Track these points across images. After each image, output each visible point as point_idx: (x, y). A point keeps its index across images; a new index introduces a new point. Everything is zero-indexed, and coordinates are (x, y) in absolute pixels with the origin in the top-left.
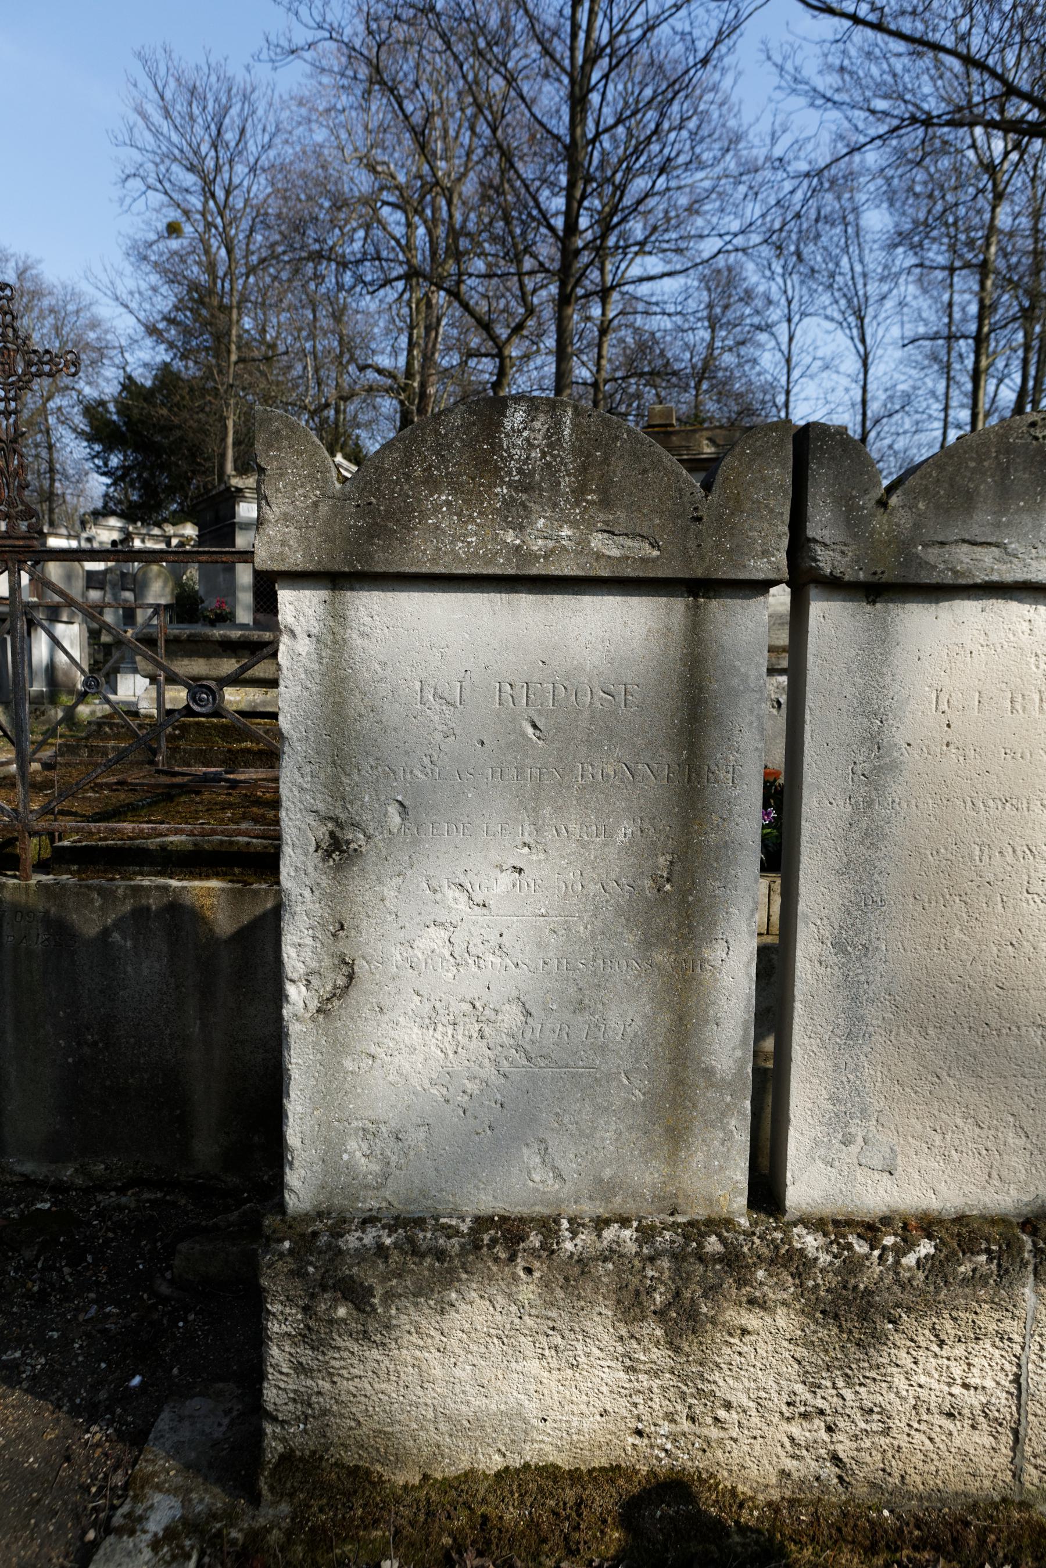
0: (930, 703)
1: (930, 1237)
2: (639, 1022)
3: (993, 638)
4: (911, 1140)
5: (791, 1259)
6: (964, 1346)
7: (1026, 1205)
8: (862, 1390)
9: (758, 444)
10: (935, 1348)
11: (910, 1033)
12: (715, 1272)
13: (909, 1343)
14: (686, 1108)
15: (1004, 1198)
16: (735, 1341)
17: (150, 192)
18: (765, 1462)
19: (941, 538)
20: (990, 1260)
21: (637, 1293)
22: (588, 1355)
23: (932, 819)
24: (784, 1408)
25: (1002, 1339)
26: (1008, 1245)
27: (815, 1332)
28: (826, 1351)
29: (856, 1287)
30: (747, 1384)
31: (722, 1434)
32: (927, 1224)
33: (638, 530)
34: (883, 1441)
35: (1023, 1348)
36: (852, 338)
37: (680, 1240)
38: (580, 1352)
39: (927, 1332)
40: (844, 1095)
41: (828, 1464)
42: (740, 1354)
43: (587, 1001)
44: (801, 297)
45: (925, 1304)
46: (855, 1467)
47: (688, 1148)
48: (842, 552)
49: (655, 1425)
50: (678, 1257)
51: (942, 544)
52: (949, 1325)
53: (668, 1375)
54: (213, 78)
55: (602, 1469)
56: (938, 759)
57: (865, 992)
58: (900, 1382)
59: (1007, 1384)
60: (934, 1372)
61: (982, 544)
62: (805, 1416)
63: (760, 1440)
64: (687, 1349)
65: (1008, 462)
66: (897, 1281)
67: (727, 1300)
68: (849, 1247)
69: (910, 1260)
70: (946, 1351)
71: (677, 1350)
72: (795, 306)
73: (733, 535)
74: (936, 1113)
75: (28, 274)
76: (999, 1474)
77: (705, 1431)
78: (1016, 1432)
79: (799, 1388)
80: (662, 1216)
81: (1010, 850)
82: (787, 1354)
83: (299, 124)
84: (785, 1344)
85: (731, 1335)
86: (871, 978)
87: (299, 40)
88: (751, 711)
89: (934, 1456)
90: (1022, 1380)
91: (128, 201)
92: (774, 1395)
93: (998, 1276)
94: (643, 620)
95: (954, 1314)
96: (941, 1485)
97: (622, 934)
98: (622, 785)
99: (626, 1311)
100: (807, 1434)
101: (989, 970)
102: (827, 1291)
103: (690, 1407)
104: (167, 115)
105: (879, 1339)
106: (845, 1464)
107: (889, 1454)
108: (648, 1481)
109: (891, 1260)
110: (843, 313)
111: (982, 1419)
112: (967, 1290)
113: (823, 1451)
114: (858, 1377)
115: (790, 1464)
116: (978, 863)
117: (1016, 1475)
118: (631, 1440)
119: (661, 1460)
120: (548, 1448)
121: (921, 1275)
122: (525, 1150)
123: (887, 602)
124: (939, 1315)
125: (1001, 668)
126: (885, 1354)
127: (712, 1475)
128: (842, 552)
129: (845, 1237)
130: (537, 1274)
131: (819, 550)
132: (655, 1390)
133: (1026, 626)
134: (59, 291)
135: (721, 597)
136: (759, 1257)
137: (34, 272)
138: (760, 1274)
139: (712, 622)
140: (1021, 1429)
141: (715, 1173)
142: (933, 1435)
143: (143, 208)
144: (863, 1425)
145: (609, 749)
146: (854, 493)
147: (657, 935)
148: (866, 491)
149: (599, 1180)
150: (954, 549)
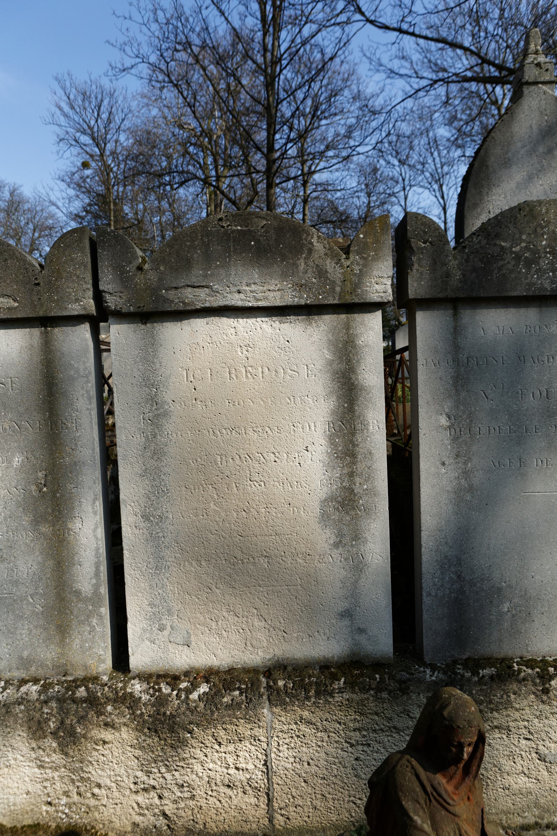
0: (183, 377)
1: (207, 682)
2: (35, 567)
3: (215, 338)
4: (198, 626)
5: (125, 699)
6: (233, 745)
7: (269, 660)
8: (176, 774)
9: (67, 241)
10: (216, 747)
11: (191, 564)
12: (83, 708)
13: (201, 745)
15: (256, 657)
16: (100, 748)
17: (72, 148)
18: (123, 818)
19: (175, 285)
20: (241, 694)
21: (39, 722)
22: (15, 759)
23: (191, 442)
24: (132, 786)
25: (255, 740)
26: (252, 685)
27: (145, 741)
28: (153, 751)
29: (164, 714)
30: (109, 773)
31: (97, 803)
32: (208, 675)
33: (5, 292)
34: (191, 803)
35: (268, 745)
36: (436, 197)
37: (63, 690)
38: (10, 758)
39: (210, 738)
40: (157, 602)
41: (161, 818)
42: (103, 755)
43: (5, 556)
44: (410, 176)
45: (207, 722)
46: (176, 819)
47: (70, 637)
48: (120, 297)
49: (59, 799)
50: (61, 700)
51: (176, 288)
52: (222, 733)
53: (63, 769)
54: (94, 87)
55: (29, 826)
56: (191, 408)
57: (163, 543)
58: (198, 768)
59: (261, 766)
60: (217, 761)
61: (198, 287)
63: (120, 805)
64: (72, 754)
65: (209, 241)
66: (188, 709)
68: (160, 690)
69: (194, 696)
71: (66, 754)
72: (407, 182)
73: (58, 292)
74: (211, 610)
75: (15, 193)
76: (261, 820)
77: (87, 801)
78: (268, 795)
79: (139, 774)
80: (59, 677)
81: (238, 457)
82: (130, 754)
83: (143, 107)
84: (129, 748)
85: (96, 744)
86: (166, 534)
87: (128, 64)
88: (83, 388)
89: (222, 811)
90: (268, 764)
91: (61, 152)
92: (125, 779)
93: (247, 703)
94: (17, 342)
95: (224, 726)
96: (227, 828)
97: (21, 517)
98: (14, 434)
99: (34, 733)
100: (147, 801)
101: (233, 526)
102: (149, 716)
103: (78, 787)
104: (72, 108)
105: (183, 743)
106: (170, 818)
107: (196, 811)
108: (56, 832)
109: (183, 696)
110: (430, 184)
111: (248, 788)
112: (229, 712)
113: (157, 811)
115: (138, 819)
116: (220, 465)
117: (271, 820)
118: (44, 808)
119: (63, 819)
121: (202, 705)
123: (152, 322)
125: (221, 355)
126: (187, 751)
127: (93, 827)
128: (120, 297)
129: (158, 684)
131: (108, 297)
132: (56, 778)
133: (233, 331)
134: (32, 200)
135: (60, 326)
136: (107, 698)
137: (18, 191)
138: (109, 708)
139: (56, 341)
140: (270, 793)
141: (87, 651)
142: (221, 799)
143: (70, 155)
144: (179, 794)
145: (5, 414)
146: (124, 264)
147: (41, 516)
148: (130, 262)
149: (21, 658)
150: (183, 291)
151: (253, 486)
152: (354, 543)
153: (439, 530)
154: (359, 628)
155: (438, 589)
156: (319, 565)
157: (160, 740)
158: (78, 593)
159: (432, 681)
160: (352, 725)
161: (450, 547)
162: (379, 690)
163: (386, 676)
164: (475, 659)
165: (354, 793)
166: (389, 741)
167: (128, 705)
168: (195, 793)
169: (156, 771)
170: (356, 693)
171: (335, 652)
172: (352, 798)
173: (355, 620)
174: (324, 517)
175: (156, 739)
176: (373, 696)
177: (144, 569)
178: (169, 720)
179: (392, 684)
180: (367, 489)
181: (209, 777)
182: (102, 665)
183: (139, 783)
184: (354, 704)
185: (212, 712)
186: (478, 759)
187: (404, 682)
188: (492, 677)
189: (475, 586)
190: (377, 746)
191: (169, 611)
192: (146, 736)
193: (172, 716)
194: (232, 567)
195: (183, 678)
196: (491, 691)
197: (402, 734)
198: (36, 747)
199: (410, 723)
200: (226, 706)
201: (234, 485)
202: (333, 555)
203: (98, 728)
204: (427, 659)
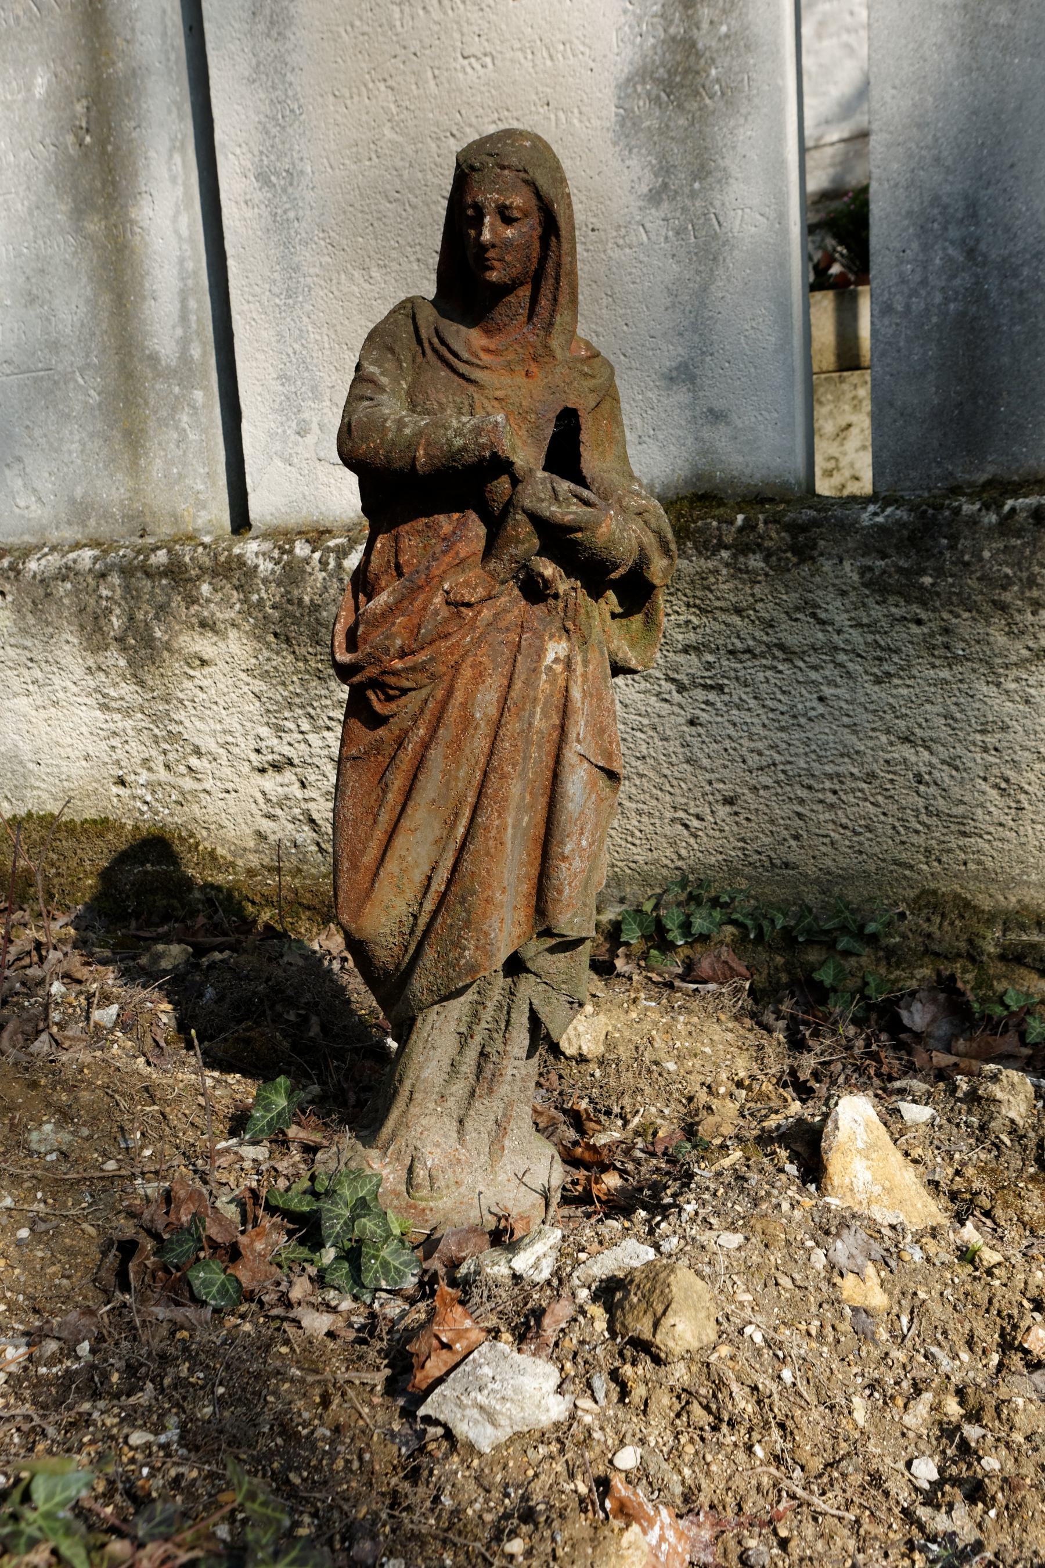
11: (352, 279)
14: (138, 406)
22: (65, 689)
24: (253, 757)
27: (269, 659)
28: (284, 684)
29: (300, 600)
31: (197, 786)
40: (292, 372)
47: (146, 454)
50: (127, 572)
53: (140, 716)
55: (95, 821)
68: (290, 552)
71: (141, 683)
79: (264, 731)
82: (246, 689)
92: (241, 740)
101: (430, 176)
102: (273, 607)
109: (332, 564)
115: (266, 825)
120: (45, 796)
122: (7, 472)
127: (192, 835)
130: (9, 598)
149: (72, 501)
151: (469, 70)
152: (697, 185)
153: (919, 126)
154: (711, 410)
155: (914, 293)
156: (615, 254)
158: (153, 359)
159: (875, 525)
160: (680, 637)
161: (948, 170)
162: (742, 549)
165: (684, 800)
166: (768, 681)
169: (293, 726)
170: (689, 558)
171: (656, 472)
172: (681, 814)
173: (702, 389)
174: (628, 125)
175: (290, 658)
176: (727, 565)
177: (264, 299)
179: (774, 535)
180: (727, 36)
182: (202, 513)
184: (683, 585)
186: (551, 281)
187: (804, 528)
189: (1015, 274)
190: (739, 692)
191: (314, 389)
193: (315, 608)
196: (1033, 553)
197: (801, 664)
198: (94, 666)
199: (820, 635)
201: (430, 74)
202: (648, 225)
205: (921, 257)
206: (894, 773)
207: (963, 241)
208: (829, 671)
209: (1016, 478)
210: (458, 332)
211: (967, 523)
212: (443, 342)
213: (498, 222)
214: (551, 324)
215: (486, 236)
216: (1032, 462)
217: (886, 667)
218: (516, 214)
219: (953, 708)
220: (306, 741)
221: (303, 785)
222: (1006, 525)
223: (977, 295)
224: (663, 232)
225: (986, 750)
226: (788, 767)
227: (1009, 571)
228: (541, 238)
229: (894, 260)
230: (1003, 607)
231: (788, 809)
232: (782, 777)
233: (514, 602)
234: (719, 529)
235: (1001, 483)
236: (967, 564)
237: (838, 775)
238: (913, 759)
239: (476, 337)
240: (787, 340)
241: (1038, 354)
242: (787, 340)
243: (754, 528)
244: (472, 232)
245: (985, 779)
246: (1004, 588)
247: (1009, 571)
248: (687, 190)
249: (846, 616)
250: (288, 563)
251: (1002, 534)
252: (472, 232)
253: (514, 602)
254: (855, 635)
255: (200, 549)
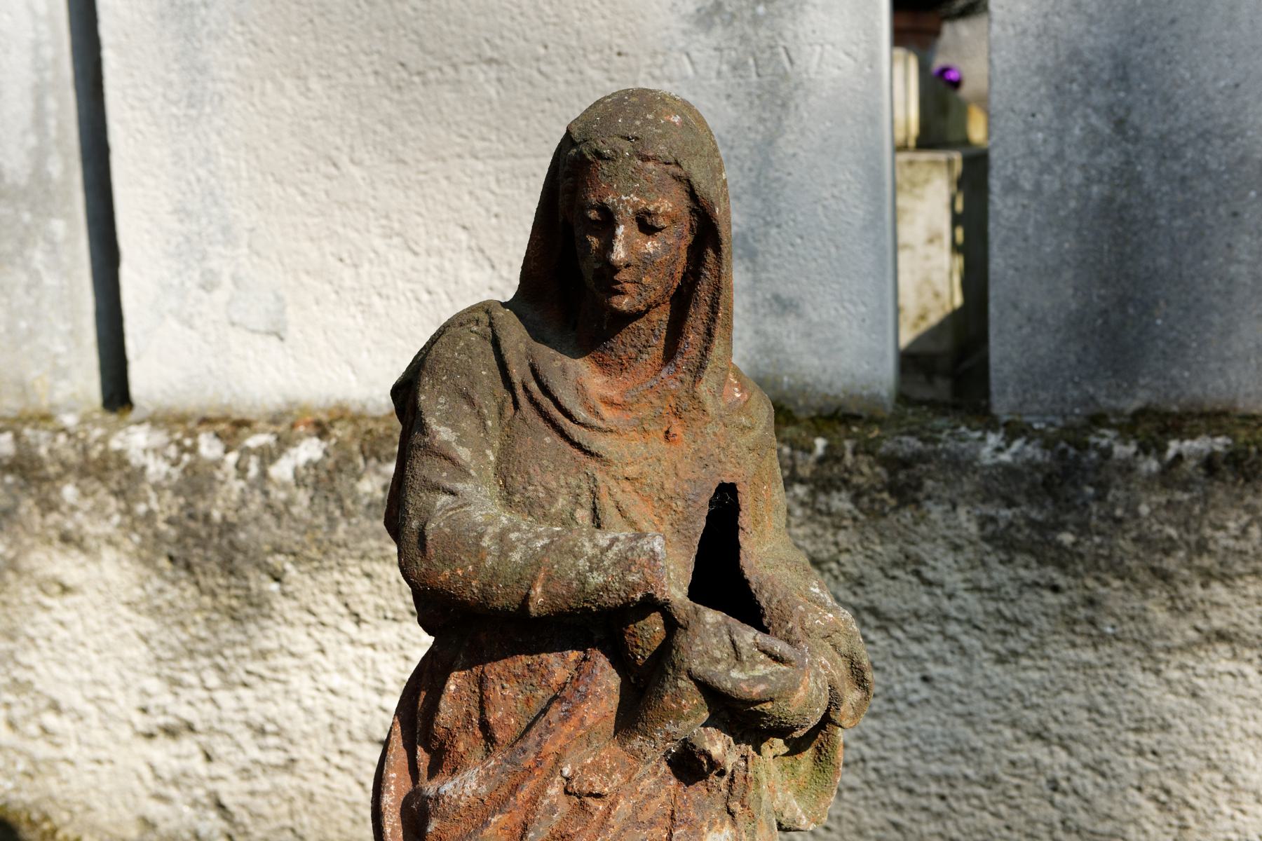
10: (349, 626)
11: (281, 89)
18: (117, 800)
24: (137, 718)
28: (182, 624)
29: (207, 518)
34: (284, 780)
39: (331, 599)
42: (62, 624)
52: (362, 585)
57: (204, 23)
58: (300, 682)
62: (170, 732)
67: (31, 534)
68: (193, 450)
69: (282, 470)
70: (366, 634)
74: (340, 230)
77: (29, 746)
79: (153, 685)
82: (126, 628)
84: (124, 610)
92: (119, 696)
105: (259, 605)
106: (232, 814)
107: (300, 803)
109: (254, 470)
114: (239, 675)
115: (155, 810)
121: (303, 496)
124: (342, 568)
127: (46, 818)
144: (255, 753)
154: (777, 298)
155: (1046, 168)
157: (202, 592)
159: (1000, 465)
161: (1091, 20)
163: (848, 444)
164: (1168, 414)
167: (113, 485)
168: (295, 755)
173: (765, 269)
175: (191, 591)
176: (803, 504)
178: (221, 534)
179: (865, 469)
181: (331, 712)
183: (153, 710)
185: (332, 521)
186: (705, 308)
187: (906, 463)
188: (1210, 464)
189: (1177, 155)
191: (226, 230)
192: (165, 578)
193: (228, 527)
194: (396, 96)
195: (261, 425)
199: (925, 599)
200: (369, 506)
202: (694, 54)
203: (46, 548)
204: (1002, 405)
205: (1055, 124)
206: (1022, 777)
207: (1110, 108)
208: (936, 644)
209: (1175, 408)
210: (564, 371)
211: (1119, 470)
212: (546, 390)
213: (635, 231)
214: (701, 367)
215: (619, 253)
216: (1197, 390)
217: (1012, 643)
218: (662, 222)
219: (1099, 699)
220: (213, 701)
221: (208, 758)
222: (1170, 474)
223: (1126, 175)
224: (715, 64)
225: (1140, 753)
226: (881, 765)
227: (1172, 532)
228: (691, 249)
229: (1021, 126)
230: (1165, 577)
231: (880, 817)
232: (873, 776)
233: (663, 780)
234: (792, 457)
235: (1156, 413)
236: (1118, 521)
237: (947, 777)
238: (1046, 760)
239: (583, 368)
240: (878, 215)
241: (1204, 257)
242: (878, 215)
243: (839, 460)
244: (594, 241)
245: (1139, 789)
246: (1167, 553)
247: (1172, 532)
248: (747, 14)
249: (958, 576)
250: (191, 466)
251: (1165, 485)
252: (594, 241)
253: (663, 780)
254: (972, 602)
255: (62, 438)
